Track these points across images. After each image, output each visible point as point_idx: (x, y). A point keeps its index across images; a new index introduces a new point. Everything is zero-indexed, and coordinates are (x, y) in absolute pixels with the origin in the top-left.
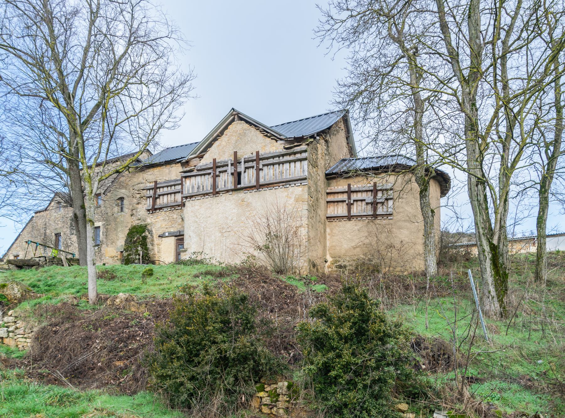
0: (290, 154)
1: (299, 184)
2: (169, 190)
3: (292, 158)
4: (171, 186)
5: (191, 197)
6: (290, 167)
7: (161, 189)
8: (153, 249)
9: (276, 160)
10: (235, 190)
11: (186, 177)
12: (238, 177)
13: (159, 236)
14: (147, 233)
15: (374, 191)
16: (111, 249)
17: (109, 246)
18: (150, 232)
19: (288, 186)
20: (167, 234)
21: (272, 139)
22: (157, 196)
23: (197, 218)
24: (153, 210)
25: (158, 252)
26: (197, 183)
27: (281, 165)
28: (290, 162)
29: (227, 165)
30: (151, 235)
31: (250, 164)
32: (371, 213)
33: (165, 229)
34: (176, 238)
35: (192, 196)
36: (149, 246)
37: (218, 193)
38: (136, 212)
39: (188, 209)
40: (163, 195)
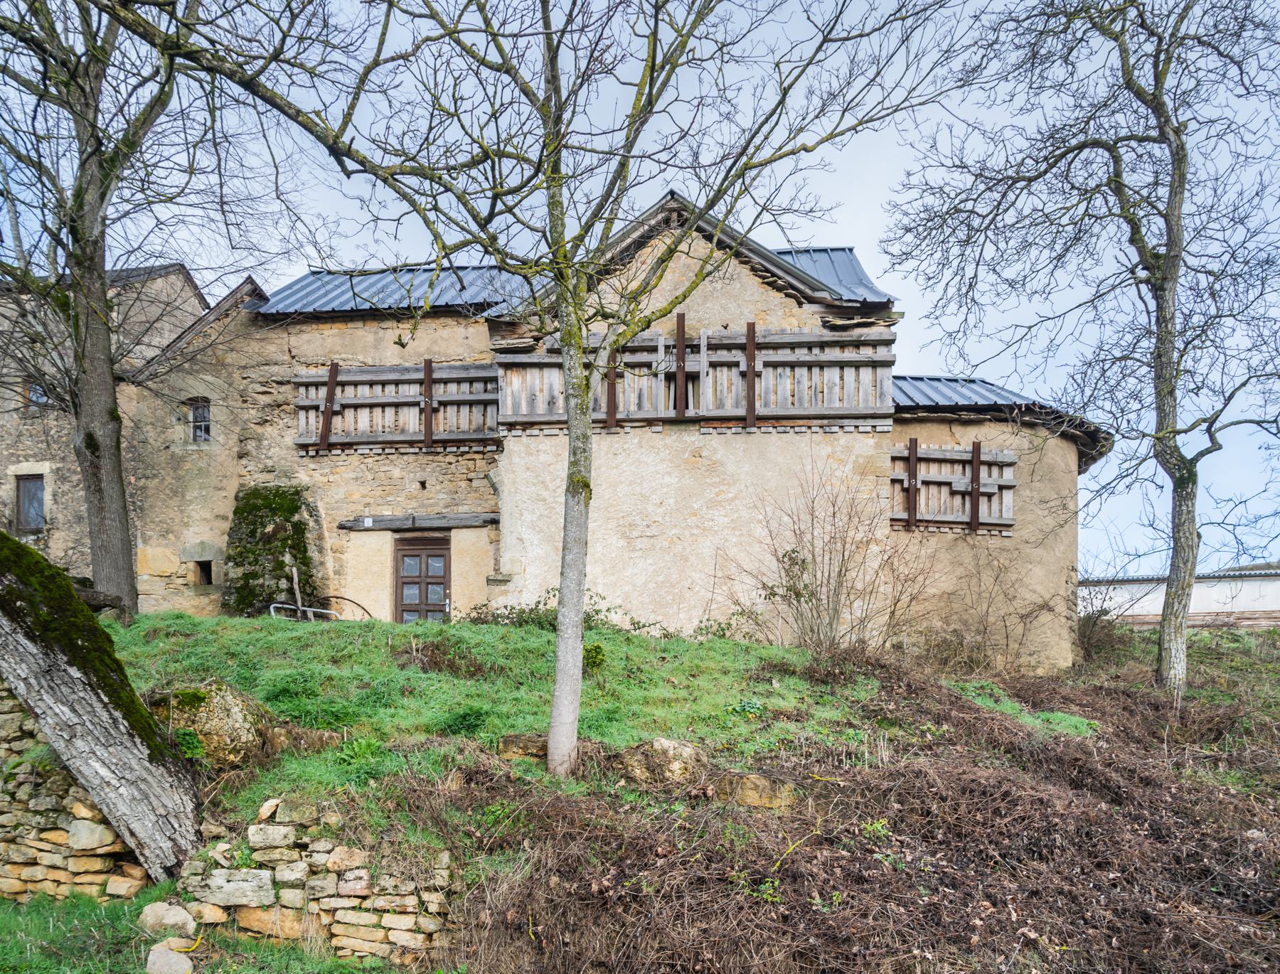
0: (842, 345)
1: (869, 429)
2: (378, 394)
3: (849, 355)
4: (383, 384)
5: (527, 425)
6: (842, 378)
7: (350, 390)
8: (322, 563)
9: (802, 354)
10: (680, 421)
11: (508, 366)
12: (682, 382)
13: (341, 527)
14: (306, 515)
15: (973, 461)
16: (159, 550)
17: (153, 542)
18: (313, 511)
19: (836, 429)
20: (368, 523)
21: (787, 295)
22: (337, 408)
23: (546, 488)
24: (324, 446)
25: (336, 573)
26: (546, 387)
27: (816, 371)
28: (842, 365)
29: (654, 349)
30: (317, 521)
31: (723, 355)
32: (966, 519)
33: (360, 507)
34: (397, 536)
35: (532, 424)
36: (313, 553)
37: (620, 423)
38: (258, 448)
39: (516, 460)
40: (356, 407)
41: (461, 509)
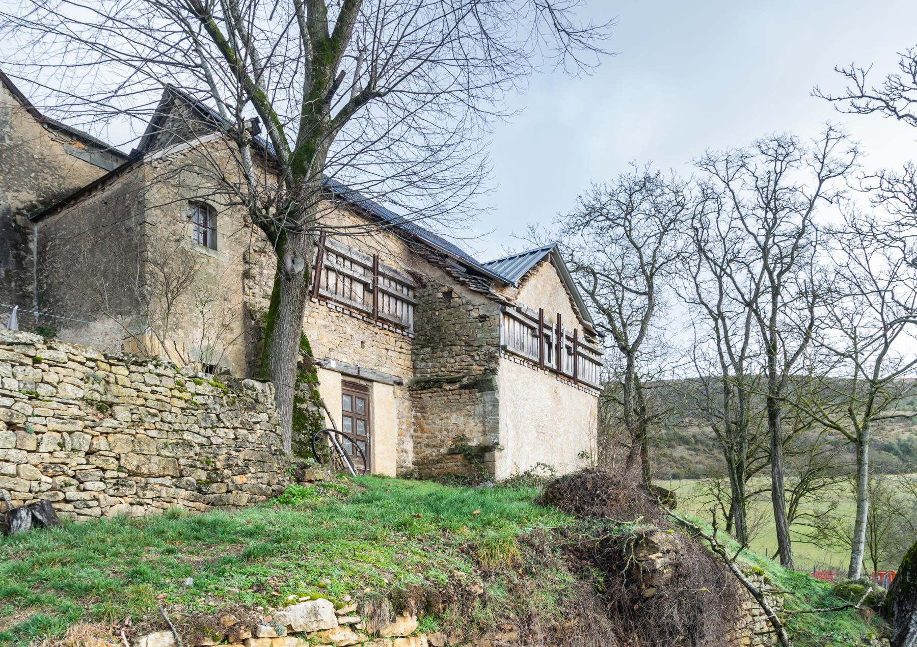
41: (384, 370)
